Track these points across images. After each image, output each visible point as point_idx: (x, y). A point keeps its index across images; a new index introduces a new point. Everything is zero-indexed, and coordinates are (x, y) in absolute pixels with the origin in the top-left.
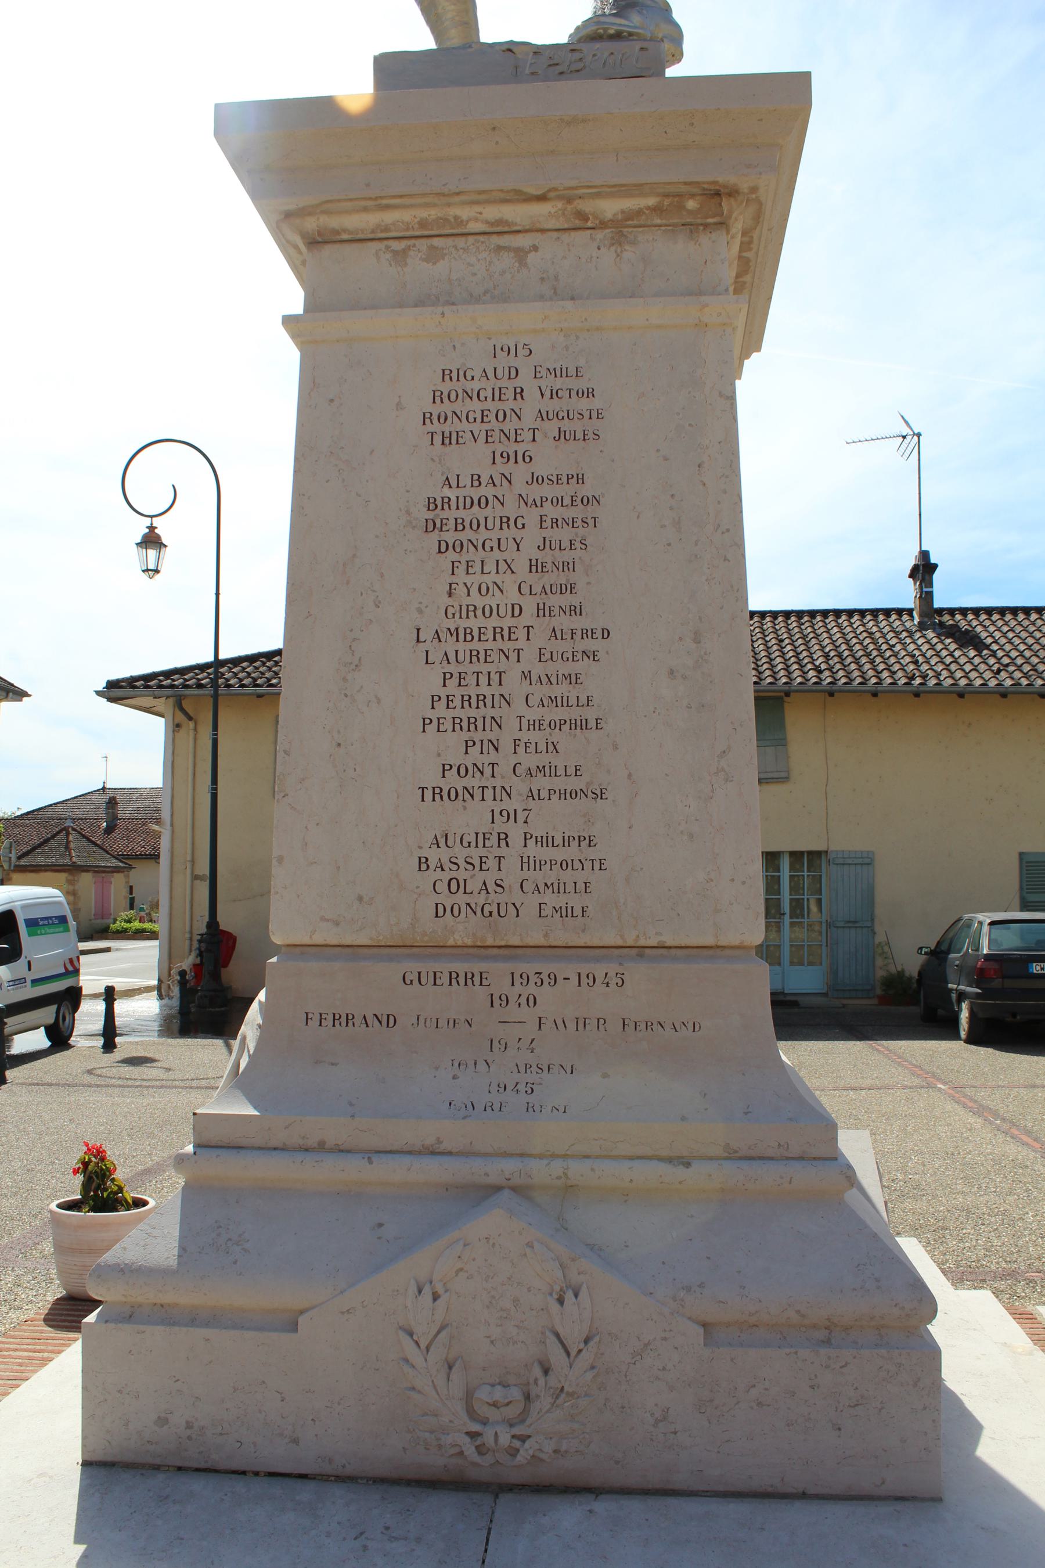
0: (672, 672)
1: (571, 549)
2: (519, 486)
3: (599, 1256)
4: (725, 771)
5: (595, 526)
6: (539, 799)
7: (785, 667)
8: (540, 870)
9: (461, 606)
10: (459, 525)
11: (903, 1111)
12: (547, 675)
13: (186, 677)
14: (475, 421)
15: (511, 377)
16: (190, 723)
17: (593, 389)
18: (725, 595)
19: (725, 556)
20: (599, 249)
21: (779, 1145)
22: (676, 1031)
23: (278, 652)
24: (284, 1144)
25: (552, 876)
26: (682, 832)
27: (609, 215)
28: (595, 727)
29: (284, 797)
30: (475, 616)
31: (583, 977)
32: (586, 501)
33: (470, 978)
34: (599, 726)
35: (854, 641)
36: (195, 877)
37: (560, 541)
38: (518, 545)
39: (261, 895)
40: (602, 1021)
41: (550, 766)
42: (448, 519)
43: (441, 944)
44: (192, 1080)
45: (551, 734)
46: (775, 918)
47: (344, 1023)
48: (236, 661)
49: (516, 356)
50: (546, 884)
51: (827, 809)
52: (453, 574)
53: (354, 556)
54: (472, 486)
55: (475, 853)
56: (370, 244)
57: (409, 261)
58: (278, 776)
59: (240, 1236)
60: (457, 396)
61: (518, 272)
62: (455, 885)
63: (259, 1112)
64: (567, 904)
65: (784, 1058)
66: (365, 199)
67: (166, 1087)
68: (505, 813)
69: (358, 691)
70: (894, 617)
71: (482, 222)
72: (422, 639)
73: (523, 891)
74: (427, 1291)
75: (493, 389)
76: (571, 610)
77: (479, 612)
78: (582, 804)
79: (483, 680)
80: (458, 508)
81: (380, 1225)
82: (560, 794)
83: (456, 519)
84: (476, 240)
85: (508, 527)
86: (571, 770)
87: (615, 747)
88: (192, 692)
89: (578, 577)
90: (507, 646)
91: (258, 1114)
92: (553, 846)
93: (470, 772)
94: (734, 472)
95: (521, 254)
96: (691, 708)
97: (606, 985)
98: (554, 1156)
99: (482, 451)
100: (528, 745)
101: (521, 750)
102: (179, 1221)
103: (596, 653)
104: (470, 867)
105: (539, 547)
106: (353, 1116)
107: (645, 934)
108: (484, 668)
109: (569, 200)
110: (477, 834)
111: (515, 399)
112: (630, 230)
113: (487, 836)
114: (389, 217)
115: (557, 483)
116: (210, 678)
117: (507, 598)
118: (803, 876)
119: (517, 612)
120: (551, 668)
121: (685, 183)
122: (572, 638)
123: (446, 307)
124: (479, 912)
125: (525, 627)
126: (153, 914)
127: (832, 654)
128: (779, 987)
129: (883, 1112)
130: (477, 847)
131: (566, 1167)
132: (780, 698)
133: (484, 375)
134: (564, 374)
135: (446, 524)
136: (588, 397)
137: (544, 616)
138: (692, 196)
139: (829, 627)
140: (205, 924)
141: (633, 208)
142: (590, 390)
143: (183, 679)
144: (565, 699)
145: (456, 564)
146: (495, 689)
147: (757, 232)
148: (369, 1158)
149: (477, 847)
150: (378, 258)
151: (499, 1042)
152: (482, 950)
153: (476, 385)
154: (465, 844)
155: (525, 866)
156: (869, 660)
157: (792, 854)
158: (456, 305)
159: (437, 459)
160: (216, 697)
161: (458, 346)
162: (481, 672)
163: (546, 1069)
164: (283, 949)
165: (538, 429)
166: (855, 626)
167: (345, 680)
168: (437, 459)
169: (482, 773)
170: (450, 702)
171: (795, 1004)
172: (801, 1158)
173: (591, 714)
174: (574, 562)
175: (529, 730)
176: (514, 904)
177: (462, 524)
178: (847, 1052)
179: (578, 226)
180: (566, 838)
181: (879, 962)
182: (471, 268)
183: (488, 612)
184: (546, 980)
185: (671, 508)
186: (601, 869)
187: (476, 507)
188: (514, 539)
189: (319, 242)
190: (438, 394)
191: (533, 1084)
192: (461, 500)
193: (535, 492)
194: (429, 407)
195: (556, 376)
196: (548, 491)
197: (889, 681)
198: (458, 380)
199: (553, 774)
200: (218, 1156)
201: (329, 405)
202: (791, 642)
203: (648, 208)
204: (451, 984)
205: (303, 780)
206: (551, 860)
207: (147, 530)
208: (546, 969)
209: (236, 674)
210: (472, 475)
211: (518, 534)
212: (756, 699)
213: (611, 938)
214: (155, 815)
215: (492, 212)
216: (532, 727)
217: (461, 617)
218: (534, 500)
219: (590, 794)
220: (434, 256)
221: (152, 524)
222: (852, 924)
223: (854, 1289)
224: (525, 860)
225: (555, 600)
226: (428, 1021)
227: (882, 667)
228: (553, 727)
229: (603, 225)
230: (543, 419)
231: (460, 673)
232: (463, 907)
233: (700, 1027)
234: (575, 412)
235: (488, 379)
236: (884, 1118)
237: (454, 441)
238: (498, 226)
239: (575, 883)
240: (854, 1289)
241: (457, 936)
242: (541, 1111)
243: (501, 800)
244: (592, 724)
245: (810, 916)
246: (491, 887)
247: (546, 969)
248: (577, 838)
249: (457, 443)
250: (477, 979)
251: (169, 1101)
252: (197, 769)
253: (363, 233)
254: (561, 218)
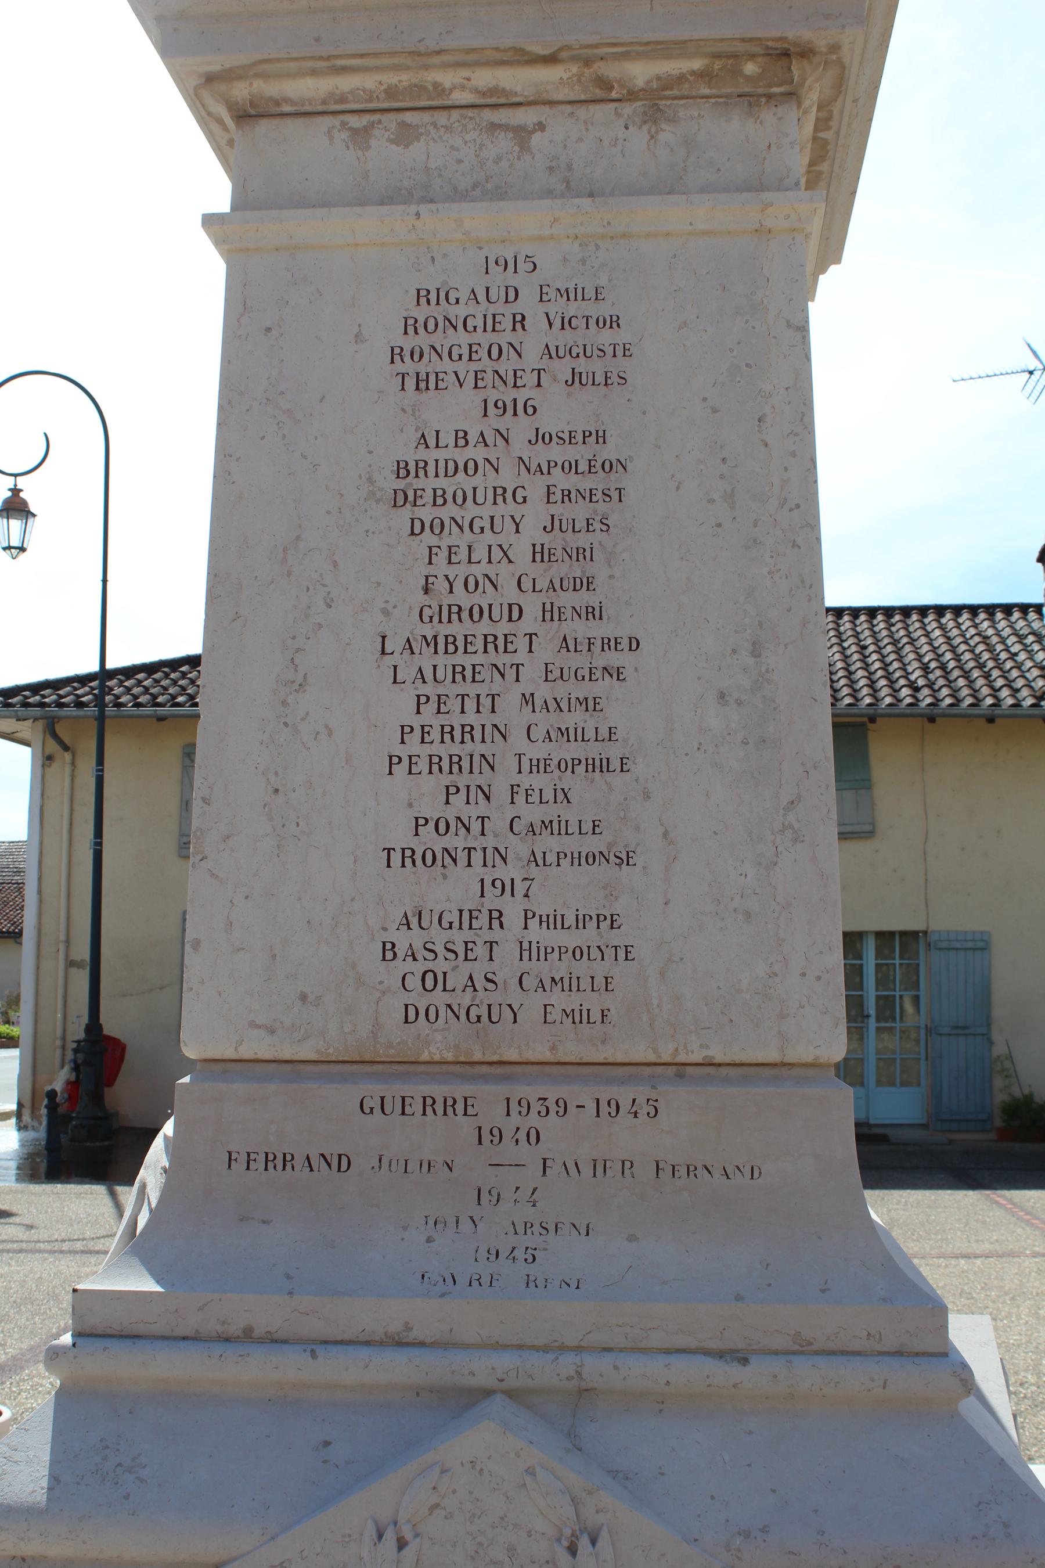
0: (722, 696)
1: (588, 531)
2: (519, 446)
3: (625, 1487)
4: (793, 829)
5: (620, 501)
6: (544, 865)
7: (869, 683)
8: (546, 960)
9: (440, 607)
10: (439, 499)
11: (1033, 1287)
12: (555, 699)
13: (61, 692)
14: (460, 358)
16: (66, 754)
17: (618, 317)
18: (793, 592)
19: (794, 540)
20: (627, 128)
21: (869, 1334)
22: (728, 1178)
23: (194, 661)
24: (197, 1331)
25: (561, 968)
26: (735, 910)
27: (640, 83)
28: (619, 769)
29: (201, 860)
30: (460, 620)
31: (603, 1105)
32: (608, 467)
33: (449, 1105)
34: (625, 768)
35: (963, 647)
36: (71, 964)
37: (574, 520)
38: (517, 525)
39: (161, 989)
40: (628, 1164)
41: (560, 821)
42: (423, 490)
43: (413, 1059)
44: (63, 1241)
45: (560, 778)
46: (857, 1022)
47: (280, 1166)
48: (129, 672)
49: (516, 272)
50: (553, 979)
51: (926, 874)
52: (430, 563)
53: (298, 538)
54: (456, 446)
55: (458, 937)
56: (320, 119)
57: (373, 142)
58: (195, 832)
59: (133, 1460)
60: (436, 325)
61: (519, 159)
62: (432, 980)
63: (163, 1287)
64: (581, 1005)
65: (874, 1216)
66: (312, 58)
67: (26, 1251)
68: (498, 883)
69: (302, 719)
70: (1016, 615)
71: (471, 92)
72: (388, 650)
73: (522, 988)
74: (390, 1535)
75: (485, 316)
76: (587, 613)
77: (465, 615)
78: (600, 871)
79: (470, 705)
80: (437, 476)
81: (327, 1444)
82: (572, 858)
83: (435, 490)
84: (462, 116)
85: (504, 500)
86: (587, 827)
87: (647, 796)
88: (69, 713)
89: (599, 569)
90: (502, 659)
91: (162, 1290)
92: (563, 928)
93: (452, 829)
94: (806, 428)
95: (522, 135)
96: (748, 743)
97: (633, 1115)
98: (563, 1348)
99: (469, 399)
100: (530, 792)
101: (520, 799)
102: (50, 1440)
103: (621, 670)
104: (452, 956)
105: (545, 528)
106: (290, 1293)
107: (685, 1047)
108: (471, 689)
109: (587, 62)
110: (461, 911)
111: (514, 329)
112: (669, 102)
113: (474, 914)
114: (346, 83)
115: (570, 443)
116: (94, 695)
117: (502, 595)
118: (894, 964)
119: (515, 615)
120: (561, 690)
121: (743, 40)
122: (589, 650)
123: (421, 206)
124: (463, 1017)
125: (526, 635)
126: (11, 1013)
127: (933, 665)
128: (862, 1116)
129: (1007, 1288)
130: (461, 928)
131: (579, 1364)
132: (863, 725)
133: (472, 296)
134: (579, 297)
135: (421, 497)
136: (611, 327)
137: (552, 620)
138: (752, 57)
139: (929, 628)
140: (83, 1027)
141: (673, 73)
142: (615, 318)
143: (58, 695)
144: (579, 731)
145: (434, 550)
146: (486, 718)
147: (838, 104)
148: (312, 1351)
149: (461, 928)
150: (331, 138)
151: (490, 1192)
152: (467, 1067)
153: (462, 311)
154: (446, 925)
155: (526, 954)
156: (983, 674)
157: (879, 935)
158: (435, 203)
159: (409, 410)
160: (101, 720)
161: (438, 258)
162: (468, 695)
163: (552, 1229)
164: (199, 1066)
165: (544, 370)
166: (964, 628)
167: (285, 703)
168: (409, 410)
169: (468, 830)
170: (426, 735)
171: (884, 1139)
172: (899, 1353)
173: (614, 752)
174: (592, 548)
175: (531, 772)
176: (510, 1006)
177: (442, 496)
178: (956, 1205)
179: (598, 97)
180: (581, 917)
181: (998, 1082)
182: (456, 153)
183: (476, 614)
184: (553, 1108)
185: (722, 477)
186: (626, 959)
187: (461, 474)
188: (512, 517)
189: (251, 116)
190: (411, 322)
191: (535, 1249)
192: (442, 464)
193: (542, 454)
194: (399, 340)
195: (568, 299)
196: (557, 453)
197: (1010, 701)
198: (438, 303)
199: (563, 831)
200: (105, 1349)
201: (265, 335)
202: (877, 649)
203: (693, 73)
204: (424, 1114)
205: (228, 837)
206: (560, 947)
207: (9, 494)
208: (553, 1093)
209: (128, 690)
210: (457, 431)
211: (518, 511)
212: (835, 725)
213: (640, 1052)
214: (16, 878)
215: (484, 78)
216: (535, 769)
217: (440, 621)
218: (539, 465)
219: (612, 859)
220: (405, 136)
221: (16, 485)
222: (961, 1029)
223: (974, 1538)
224: (526, 946)
225: (566, 599)
226: (394, 1163)
227: (1000, 682)
228: (563, 768)
229: (632, 95)
230: (551, 357)
231: (439, 696)
232: (442, 1010)
233: (760, 1173)
234: (595, 348)
235: (478, 303)
236: (1007, 1298)
237: (432, 385)
238: (491, 96)
239: (592, 978)
240: (974, 1538)
241: (433, 1049)
242: (546, 1287)
243: (494, 866)
244: (615, 764)
245: (904, 1018)
246: (480, 983)
247: (553, 1093)
248: (595, 918)
249: (437, 388)
250: (460, 1107)
251: (31, 1271)
253: (310, 104)
254: (576, 86)
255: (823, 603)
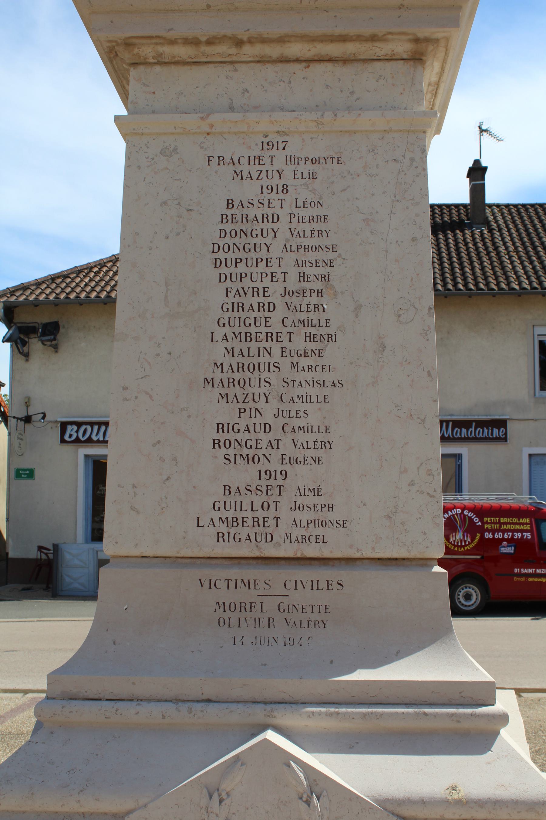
15: (274, 221)
23: (114, 260)
34: (327, 401)
41: (307, 396)
74: (216, 797)
92: (310, 402)
198: (228, 432)
211: (275, 226)
252: (11, 623)
255: (426, 195)
